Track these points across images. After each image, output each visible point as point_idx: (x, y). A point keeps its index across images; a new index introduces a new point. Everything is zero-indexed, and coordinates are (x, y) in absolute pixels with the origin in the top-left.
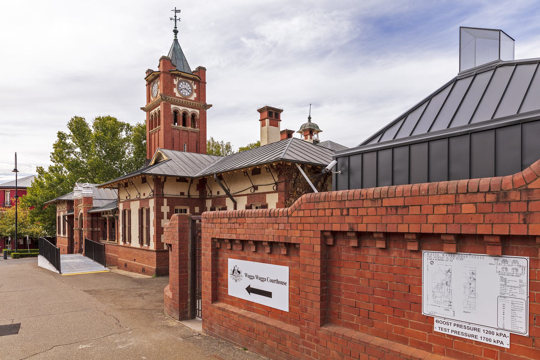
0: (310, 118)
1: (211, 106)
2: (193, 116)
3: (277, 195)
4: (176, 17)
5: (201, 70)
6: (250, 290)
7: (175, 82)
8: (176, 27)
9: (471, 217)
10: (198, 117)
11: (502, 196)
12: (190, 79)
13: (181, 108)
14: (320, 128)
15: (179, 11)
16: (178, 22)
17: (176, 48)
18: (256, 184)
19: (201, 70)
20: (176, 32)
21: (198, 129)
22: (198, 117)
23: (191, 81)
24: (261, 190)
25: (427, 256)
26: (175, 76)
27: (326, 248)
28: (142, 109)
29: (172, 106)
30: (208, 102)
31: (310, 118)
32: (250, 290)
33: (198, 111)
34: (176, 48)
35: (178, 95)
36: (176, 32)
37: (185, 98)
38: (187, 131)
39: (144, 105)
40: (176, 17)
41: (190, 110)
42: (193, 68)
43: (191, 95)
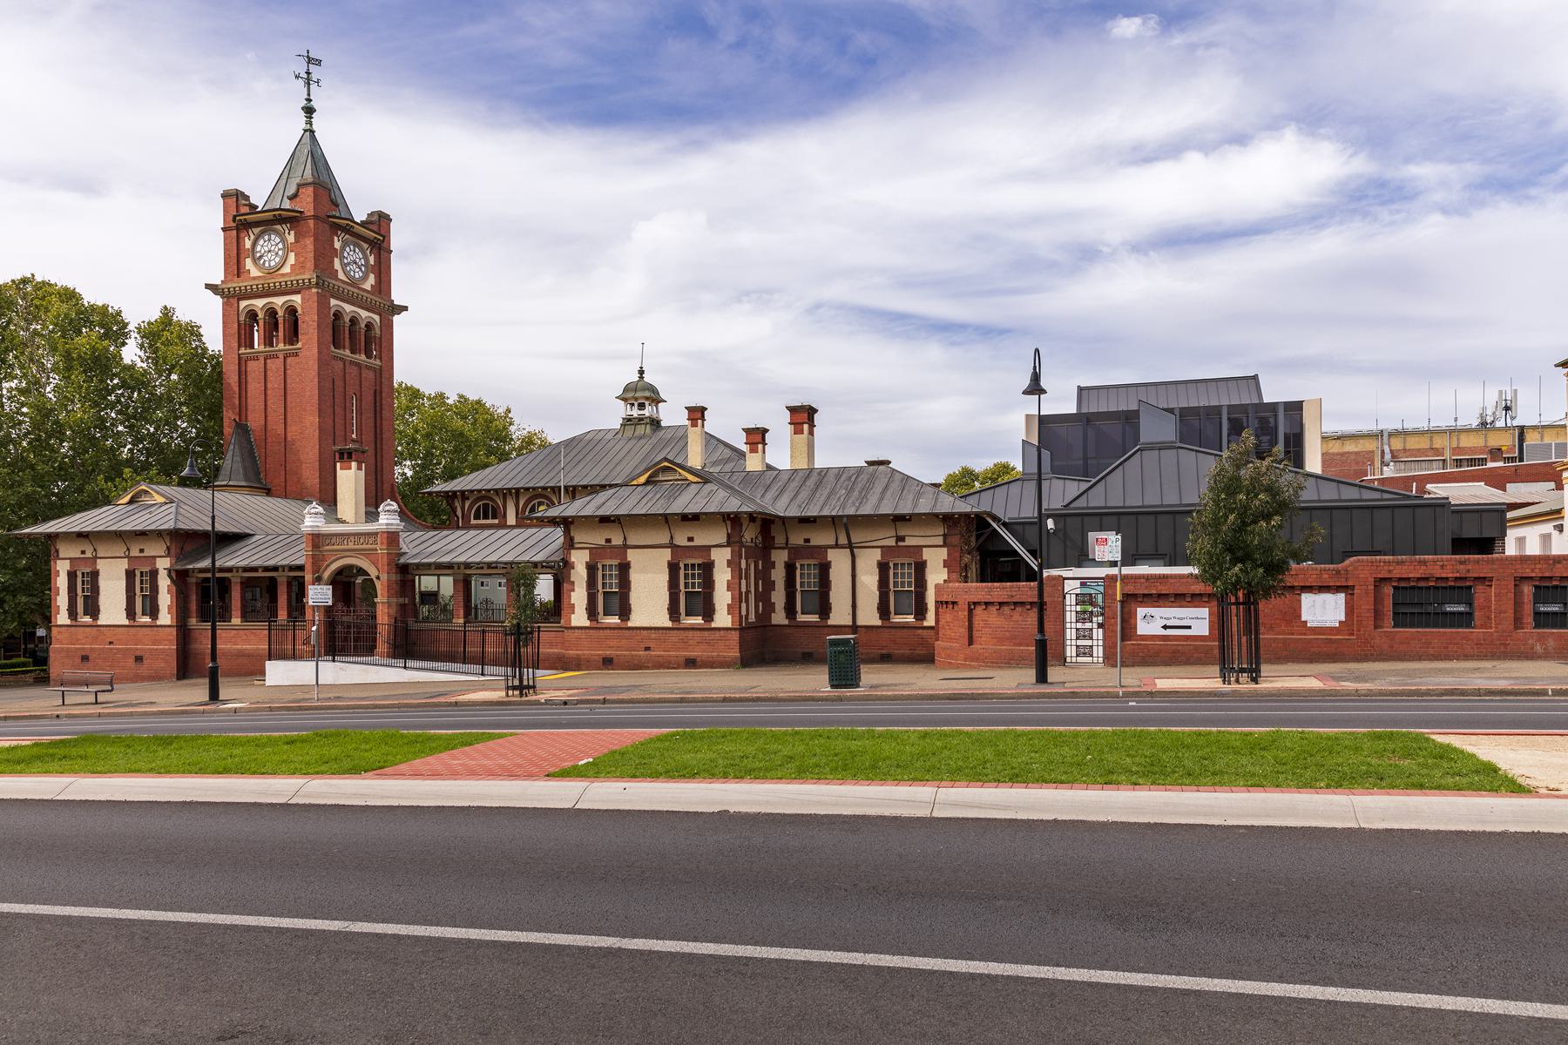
0: (641, 372)
1: (405, 308)
2: (369, 326)
3: (945, 550)
4: (308, 73)
5: (380, 221)
6: (1165, 627)
7: (337, 245)
8: (309, 100)
9: (1326, 579)
10: (378, 331)
11: (1338, 572)
12: (365, 239)
13: (348, 308)
14: (663, 396)
15: (319, 63)
16: (313, 87)
17: (311, 151)
18: (901, 533)
19: (380, 221)
20: (309, 111)
21: (378, 362)
22: (378, 331)
23: (365, 246)
24: (909, 542)
25: (1304, 596)
26: (336, 228)
27: (970, 611)
28: (208, 286)
29: (333, 302)
30: (397, 298)
31: (641, 372)
32: (1165, 627)
33: (377, 318)
34: (311, 151)
35: (341, 276)
36: (309, 111)
37: (354, 283)
38: (358, 365)
39: (218, 277)
40: (308, 73)
41: (364, 314)
42: (359, 216)
43: (365, 278)
